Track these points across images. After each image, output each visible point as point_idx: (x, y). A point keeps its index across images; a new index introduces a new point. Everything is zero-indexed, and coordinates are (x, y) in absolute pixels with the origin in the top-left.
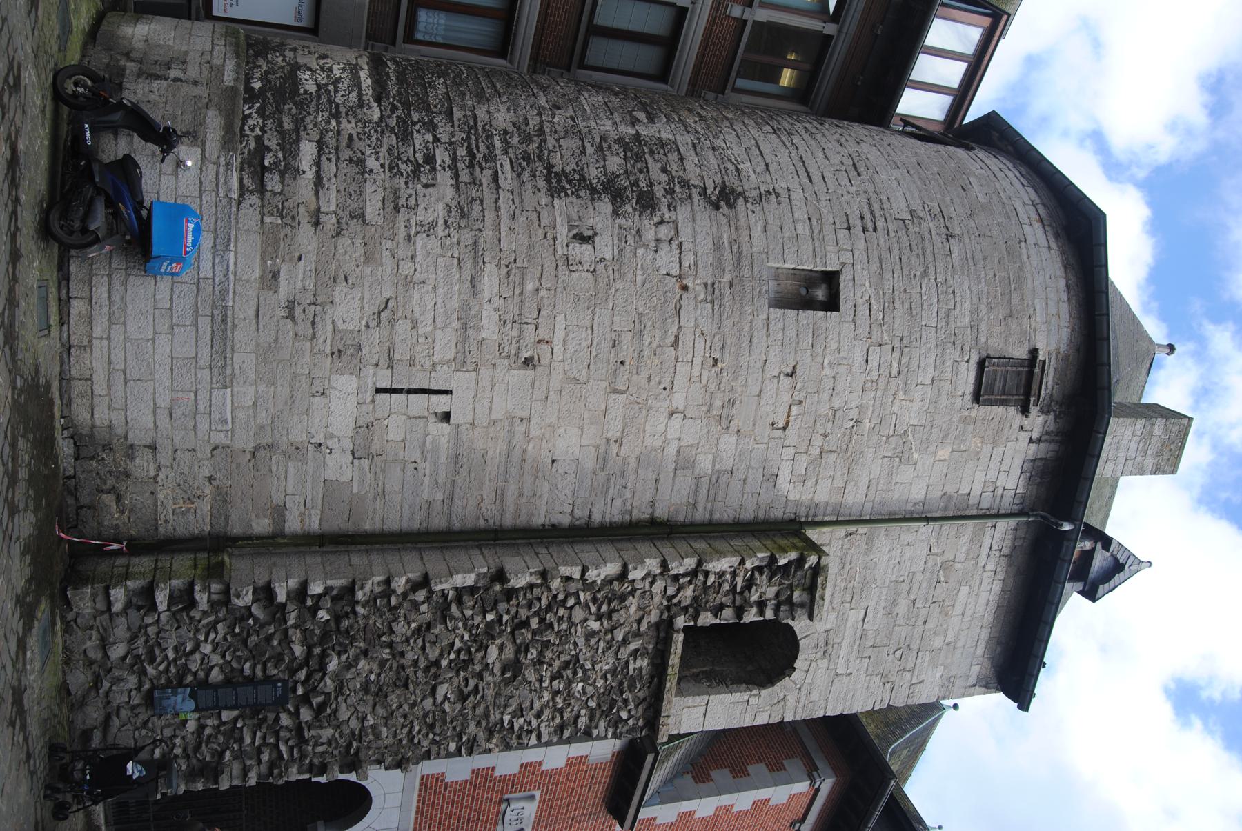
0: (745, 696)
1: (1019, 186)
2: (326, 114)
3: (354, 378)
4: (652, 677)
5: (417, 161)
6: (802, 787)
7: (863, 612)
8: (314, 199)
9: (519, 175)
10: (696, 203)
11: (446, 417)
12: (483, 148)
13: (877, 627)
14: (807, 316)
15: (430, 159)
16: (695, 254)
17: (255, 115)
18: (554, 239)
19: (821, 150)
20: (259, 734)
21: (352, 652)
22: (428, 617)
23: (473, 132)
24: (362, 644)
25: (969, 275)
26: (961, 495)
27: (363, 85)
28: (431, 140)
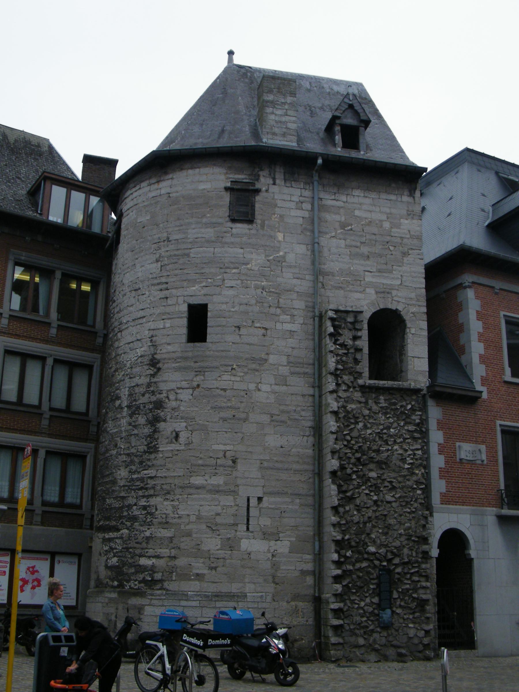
1: (140, 192)
2: (127, 553)
3: (242, 541)
4: (390, 394)
5: (145, 514)
7: (366, 273)
8: (164, 559)
9: (149, 466)
10: (158, 380)
11: (260, 499)
12: (138, 483)
15: (145, 508)
16: (182, 381)
17: (129, 584)
18: (178, 450)
19: (129, 308)
20: (406, 581)
21: (367, 540)
22: (352, 506)
25: (188, 229)
27: (113, 536)
28: (136, 507)
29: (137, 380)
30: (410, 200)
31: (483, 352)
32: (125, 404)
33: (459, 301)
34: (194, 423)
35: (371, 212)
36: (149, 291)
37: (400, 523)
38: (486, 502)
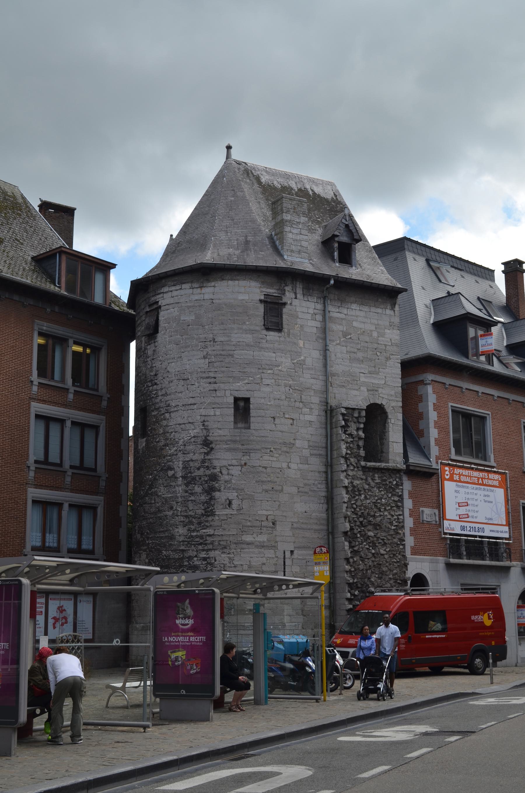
0: (391, 425)
4: (382, 472)
5: (206, 564)
6: (430, 389)
7: (361, 374)
9: (207, 527)
10: (212, 457)
11: (292, 552)
13: (367, 367)
14: (253, 413)
15: (205, 559)
16: (232, 459)
18: (231, 514)
21: (368, 583)
22: (358, 558)
23: (191, 543)
24: (366, 580)
25: (231, 334)
26: (317, 331)
28: (197, 558)
29: (191, 456)
30: (392, 313)
31: (437, 437)
32: (179, 474)
33: (419, 394)
34: (243, 493)
35: (364, 323)
36: (198, 383)
37: (391, 570)
38: (438, 553)
